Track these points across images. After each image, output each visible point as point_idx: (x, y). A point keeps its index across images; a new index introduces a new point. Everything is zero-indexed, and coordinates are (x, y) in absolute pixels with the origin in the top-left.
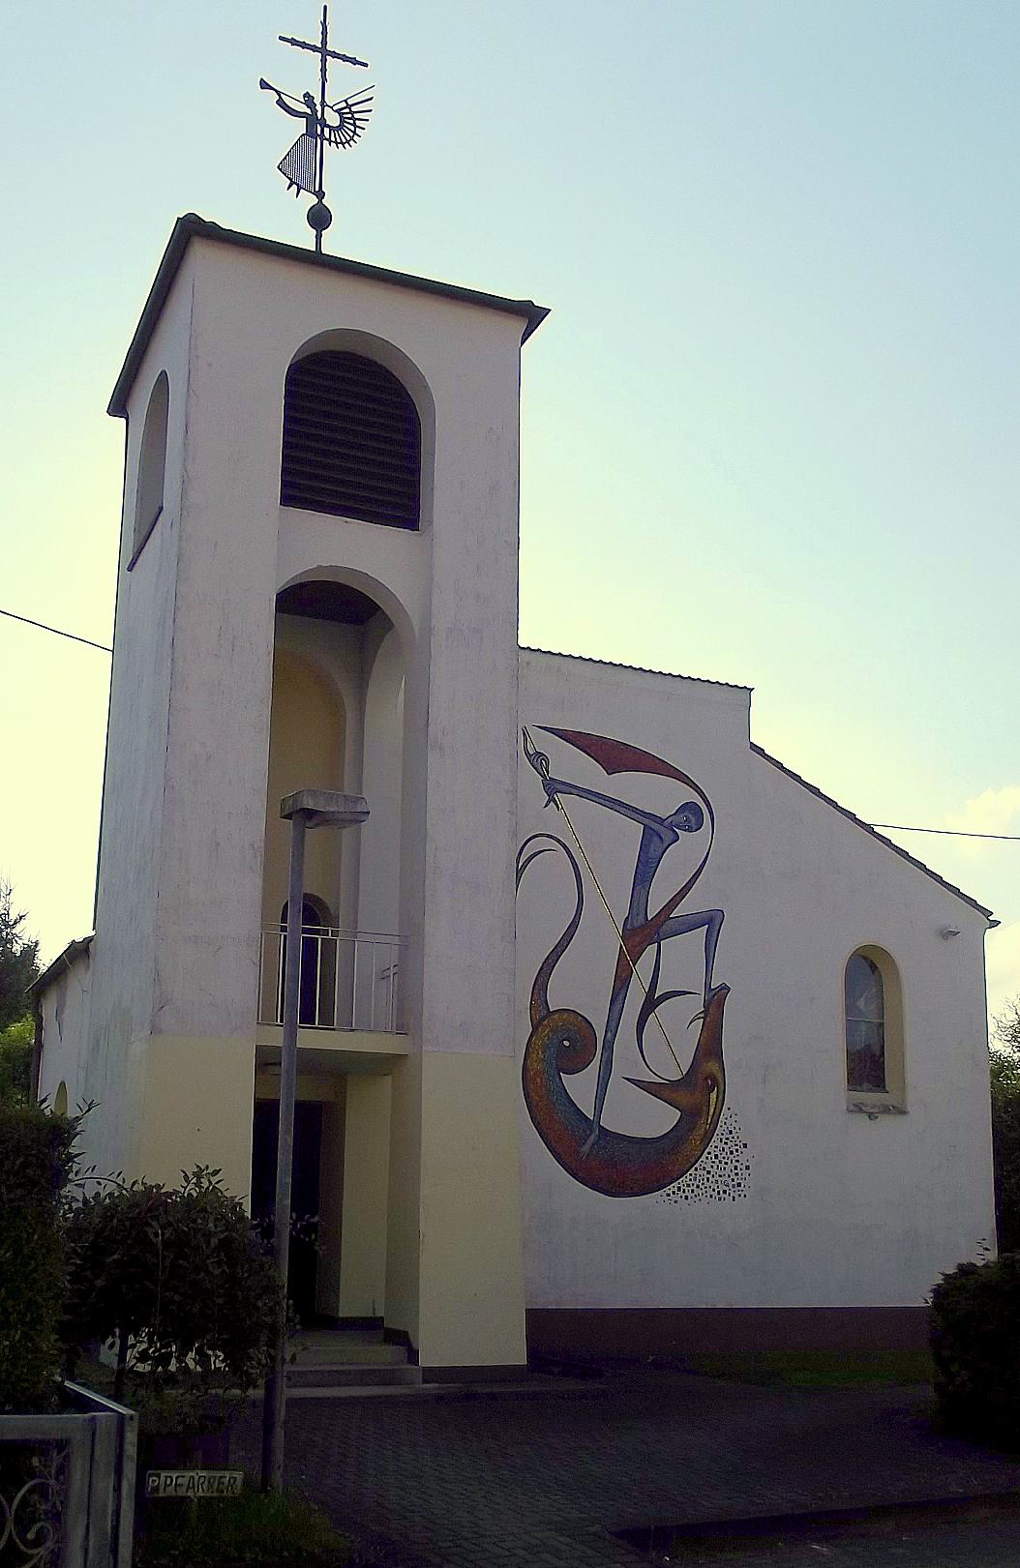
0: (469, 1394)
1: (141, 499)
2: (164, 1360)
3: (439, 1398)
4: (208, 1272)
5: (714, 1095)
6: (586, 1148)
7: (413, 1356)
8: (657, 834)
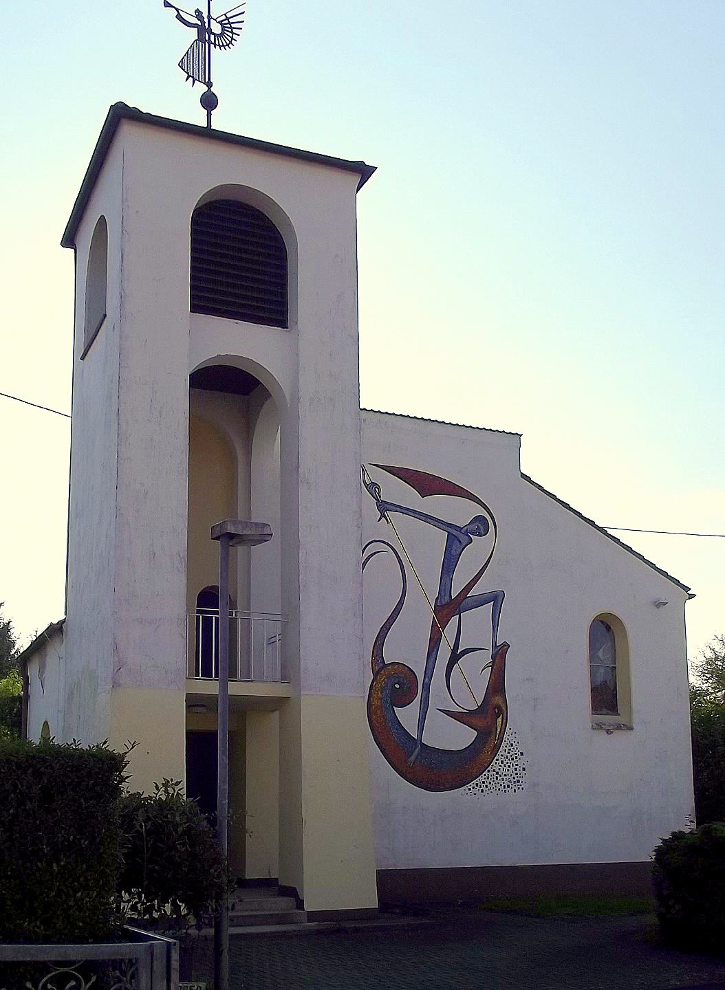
0: (340, 929)
1: (88, 309)
2: (148, 910)
3: (320, 932)
4: (177, 850)
5: (500, 720)
6: (413, 758)
7: (300, 904)
8: (457, 539)
